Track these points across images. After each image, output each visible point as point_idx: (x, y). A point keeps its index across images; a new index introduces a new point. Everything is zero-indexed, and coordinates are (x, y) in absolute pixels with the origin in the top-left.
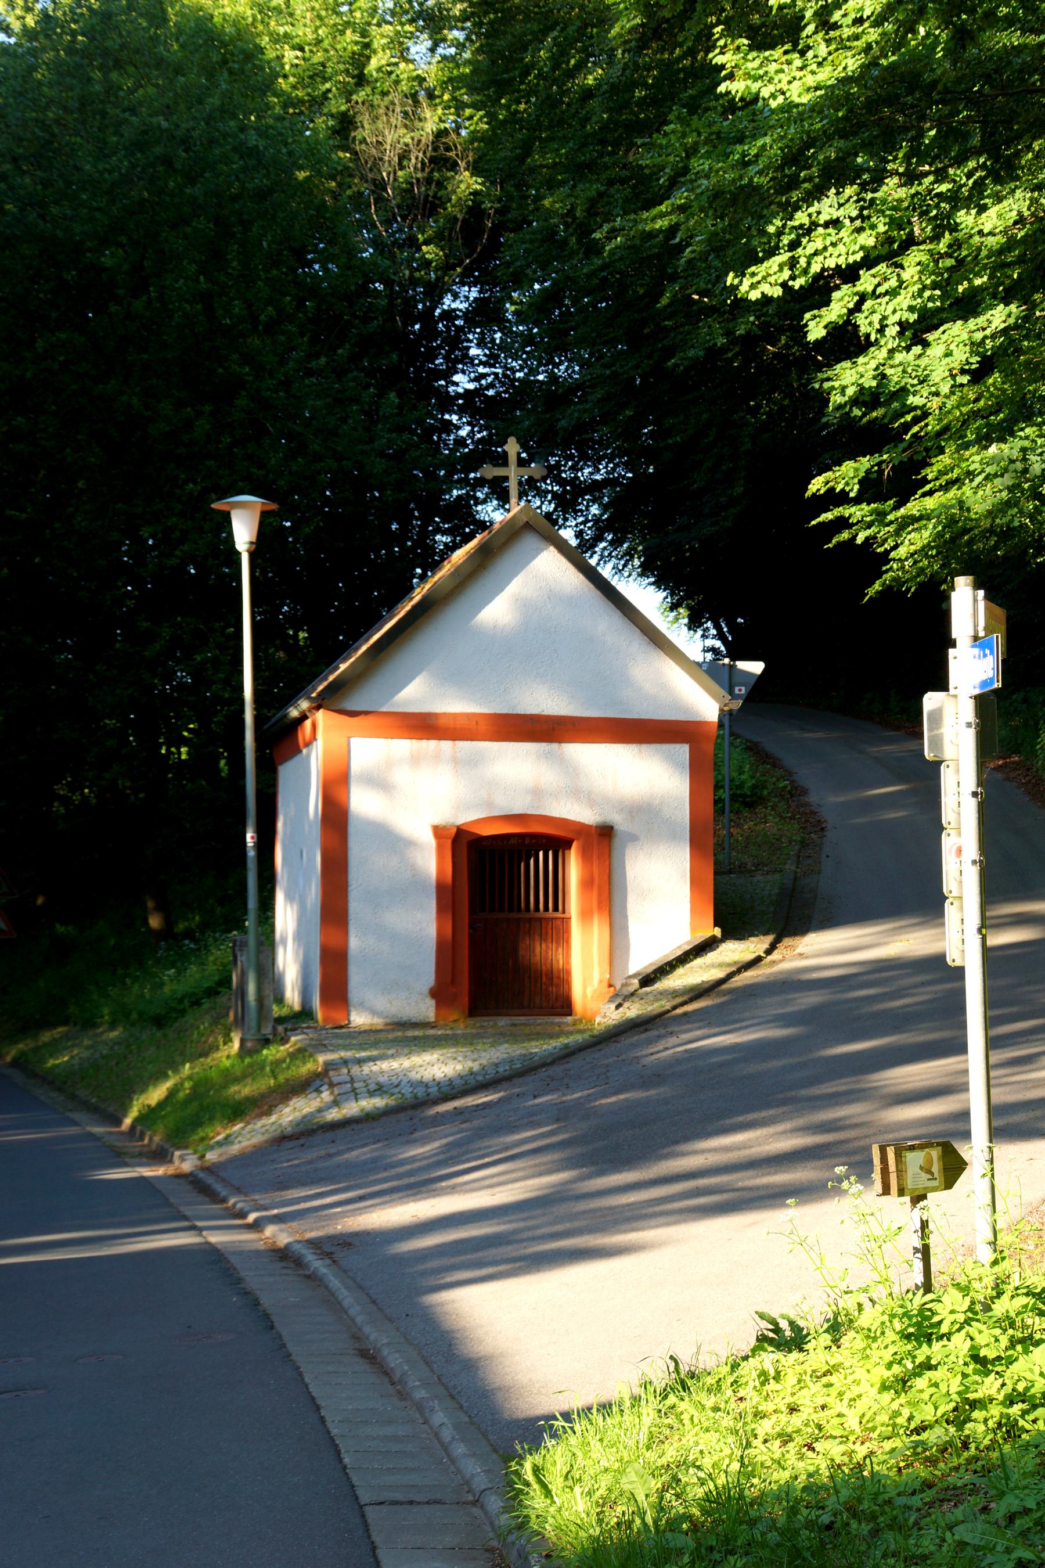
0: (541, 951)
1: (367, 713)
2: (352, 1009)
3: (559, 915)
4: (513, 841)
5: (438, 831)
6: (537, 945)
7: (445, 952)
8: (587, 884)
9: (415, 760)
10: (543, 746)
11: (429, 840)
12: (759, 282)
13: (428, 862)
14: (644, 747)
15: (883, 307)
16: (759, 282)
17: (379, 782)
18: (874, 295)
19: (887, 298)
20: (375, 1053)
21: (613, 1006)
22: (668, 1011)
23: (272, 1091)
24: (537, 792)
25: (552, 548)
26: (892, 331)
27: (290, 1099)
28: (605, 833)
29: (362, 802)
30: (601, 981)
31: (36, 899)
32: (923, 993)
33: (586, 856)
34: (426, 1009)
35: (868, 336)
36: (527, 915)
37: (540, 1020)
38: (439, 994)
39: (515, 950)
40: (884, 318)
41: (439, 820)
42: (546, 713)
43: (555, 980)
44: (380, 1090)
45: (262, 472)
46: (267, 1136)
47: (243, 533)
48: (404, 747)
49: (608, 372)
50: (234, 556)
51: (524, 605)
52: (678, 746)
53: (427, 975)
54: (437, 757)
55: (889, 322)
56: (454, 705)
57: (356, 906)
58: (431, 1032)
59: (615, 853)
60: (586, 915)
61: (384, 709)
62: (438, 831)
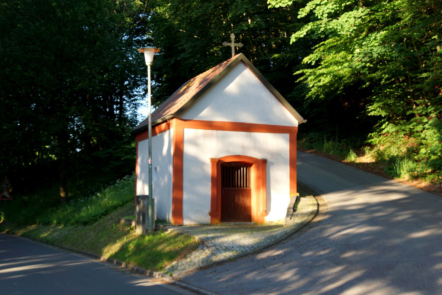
0: (242, 200)
1: (189, 120)
3: (247, 188)
4: (233, 164)
5: (213, 160)
6: (241, 198)
7: (213, 199)
8: (258, 178)
9: (205, 136)
10: (248, 133)
11: (209, 162)
13: (209, 170)
15: (323, 8)
17: (194, 143)
18: (320, 5)
19: (324, 6)
20: (218, 234)
21: (289, 219)
22: (311, 221)
23: (182, 249)
24: (243, 147)
25: (248, 69)
26: (326, 15)
27: (191, 252)
28: (264, 162)
29: (188, 149)
30: (263, 210)
32: (405, 215)
33: (258, 168)
34: (207, 219)
35: (317, 17)
36: (238, 189)
37: (243, 223)
38: (212, 214)
39: (234, 200)
40: (324, 11)
41: (213, 156)
43: (246, 210)
44: (227, 249)
45: (103, 64)
46: (195, 267)
47: (148, 59)
48: (201, 132)
49: (193, 45)
50: (146, 67)
51: (241, 87)
54: (212, 136)
55: (324, 13)
56: (219, 119)
58: (210, 227)
59: (267, 168)
60: (258, 188)
61: (195, 119)
62: (213, 160)
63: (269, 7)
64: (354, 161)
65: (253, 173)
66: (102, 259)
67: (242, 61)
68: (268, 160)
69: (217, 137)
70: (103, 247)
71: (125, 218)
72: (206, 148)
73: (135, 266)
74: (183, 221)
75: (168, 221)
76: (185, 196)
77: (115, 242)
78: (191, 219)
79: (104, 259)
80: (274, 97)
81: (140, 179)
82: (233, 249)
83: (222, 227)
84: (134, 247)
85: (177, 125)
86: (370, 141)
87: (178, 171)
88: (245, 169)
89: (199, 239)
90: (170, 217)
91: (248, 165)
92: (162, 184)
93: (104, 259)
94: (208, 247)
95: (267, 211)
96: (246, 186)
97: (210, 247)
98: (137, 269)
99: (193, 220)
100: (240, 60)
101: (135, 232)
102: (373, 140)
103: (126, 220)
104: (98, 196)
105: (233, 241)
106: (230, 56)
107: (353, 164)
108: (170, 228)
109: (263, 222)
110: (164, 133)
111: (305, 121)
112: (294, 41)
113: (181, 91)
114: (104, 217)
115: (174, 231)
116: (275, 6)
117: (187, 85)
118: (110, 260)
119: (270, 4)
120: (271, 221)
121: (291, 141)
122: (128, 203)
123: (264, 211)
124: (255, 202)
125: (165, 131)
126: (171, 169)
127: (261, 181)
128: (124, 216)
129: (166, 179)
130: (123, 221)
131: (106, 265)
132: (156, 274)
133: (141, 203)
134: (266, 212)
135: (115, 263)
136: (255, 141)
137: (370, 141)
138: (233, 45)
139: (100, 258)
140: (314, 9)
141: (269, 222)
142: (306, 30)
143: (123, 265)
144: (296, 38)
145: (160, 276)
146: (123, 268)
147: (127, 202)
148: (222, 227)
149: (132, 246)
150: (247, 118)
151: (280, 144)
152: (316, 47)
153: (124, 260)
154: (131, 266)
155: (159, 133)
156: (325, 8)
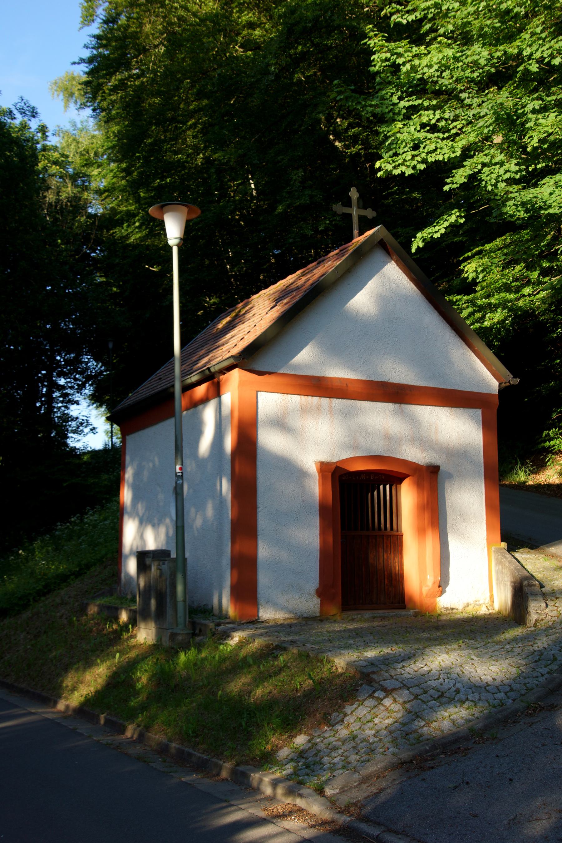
1: (270, 373)
2: (261, 607)
6: (381, 554)
9: (304, 410)
10: (397, 406)
11: (312, 468)
12: (399, 165)
13: (315, 488)
14: (454, 409)
15: (496, 171)
16: (399, 165)
17: (280, 423)
19: (498, 166)
23: (310, 696)
24: (388, 437)
25: (393, 262)
27: (340, 708)
29: (269, 440)
31: (46, 382)
33: (419, 485)
34: (311, 604)
38: (323, 593)
42: (391, 381)
48: (295, 400)
50: (171, 248)
52: (474, 410)
53: (313, 582)
54: (318, 409)
56: (337, 372)
57: (263, 522)
60: (421, 531)
61: (281, 371)
62: (323, 467)
63: (379, 174)
64: (525, 482)
65: (408, 498)
66: (61, 706)
67: (382, 245)
68: (441, 468)
69: (331, 411)
70: (59, 675)
71: (98, 602)
72: (309, 438)
73: (170, 741)
74: (258, 612)
75: (216, 611)
76: (264, 551)
77: (89, 664)
78: (276, 606)
79: (67, 707)
80: (448, 327)
81: (131, 516)
82: (461, 696)
83: (351, 626)
84: (150, 679)
85: (241, 384)
86: (547, 444)
87: (246, 490)
88: (388, 486)
89: (349, 664)
90: (227, 604)
91: (396, 479)
92: (199, 522)
93: (67, 707)
94: (388, 692)
95: (442, 585)
96: (392, 528)
97: (394, 690)
98: (180, 752)
99: (283, 608)
100: (376, 242)
101: (134, 636)
102: (552, 443)
103: (102, 608)
104: (20, 555)
105: (447, 672)
106: (352, 238)
107: (522, 486)
108: (235, 630)
109: (434, 608)
110: (200, 407)
111: (517, 381)
112: (421, 245)
113: (220, 326)
114: (43, 598)
115: (253, 637)
116: (391, 171)
117: (233, 314)
118: (86, 710)
119: (380, 169)
120: (449, 606)
121: (486, 425)
122: (93, 569)
123: (437, 585)
124: (415, 564)
125: (205, 400)
126: (225, 486)
127: (427, 516)
128: (93, 598)
129: (210, 511)
130: (93, 609)
131: (83, 728)
132: (261, 781)
133: (153, 569)
134: (442, 584)
135: (102, 722)
136: (414, 422)
137: (547, 444)
138: (355, 212)
139: (56, 703)
140: (480, 172)
141: (447, 609)
142: (446, 224)
143: (130, 732)
144: (424, 240)
145: (280, 791)
146: (131, 742)
147: (88, 566)
148: (351, 626)
149: (143, 678)
150: (398, 373)
151: (459, 431)
152: (466, 255)
153: (131, 716)
154: (157, 736)
155: (187, 409)
156: (502, 171)
